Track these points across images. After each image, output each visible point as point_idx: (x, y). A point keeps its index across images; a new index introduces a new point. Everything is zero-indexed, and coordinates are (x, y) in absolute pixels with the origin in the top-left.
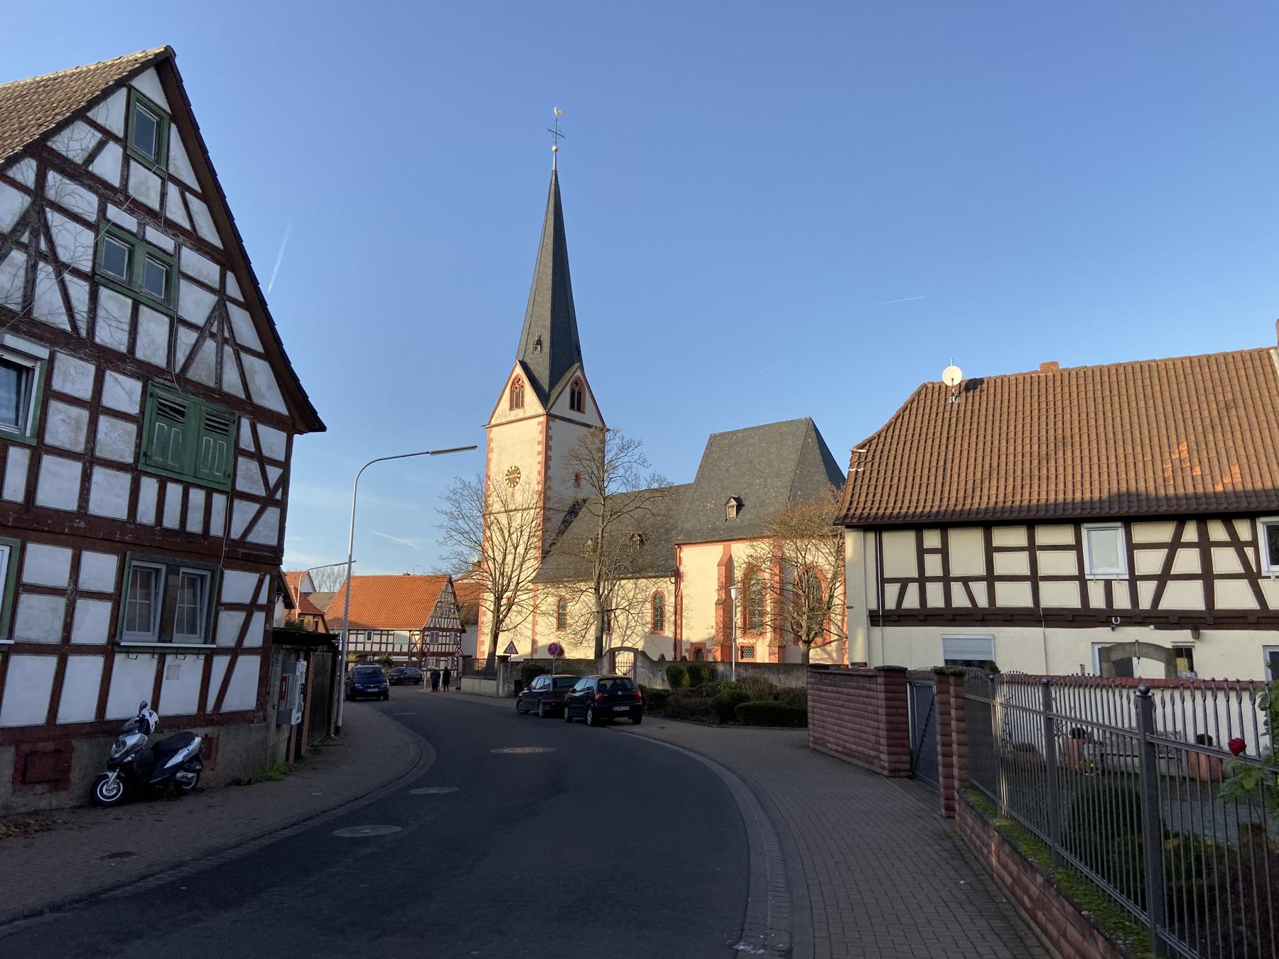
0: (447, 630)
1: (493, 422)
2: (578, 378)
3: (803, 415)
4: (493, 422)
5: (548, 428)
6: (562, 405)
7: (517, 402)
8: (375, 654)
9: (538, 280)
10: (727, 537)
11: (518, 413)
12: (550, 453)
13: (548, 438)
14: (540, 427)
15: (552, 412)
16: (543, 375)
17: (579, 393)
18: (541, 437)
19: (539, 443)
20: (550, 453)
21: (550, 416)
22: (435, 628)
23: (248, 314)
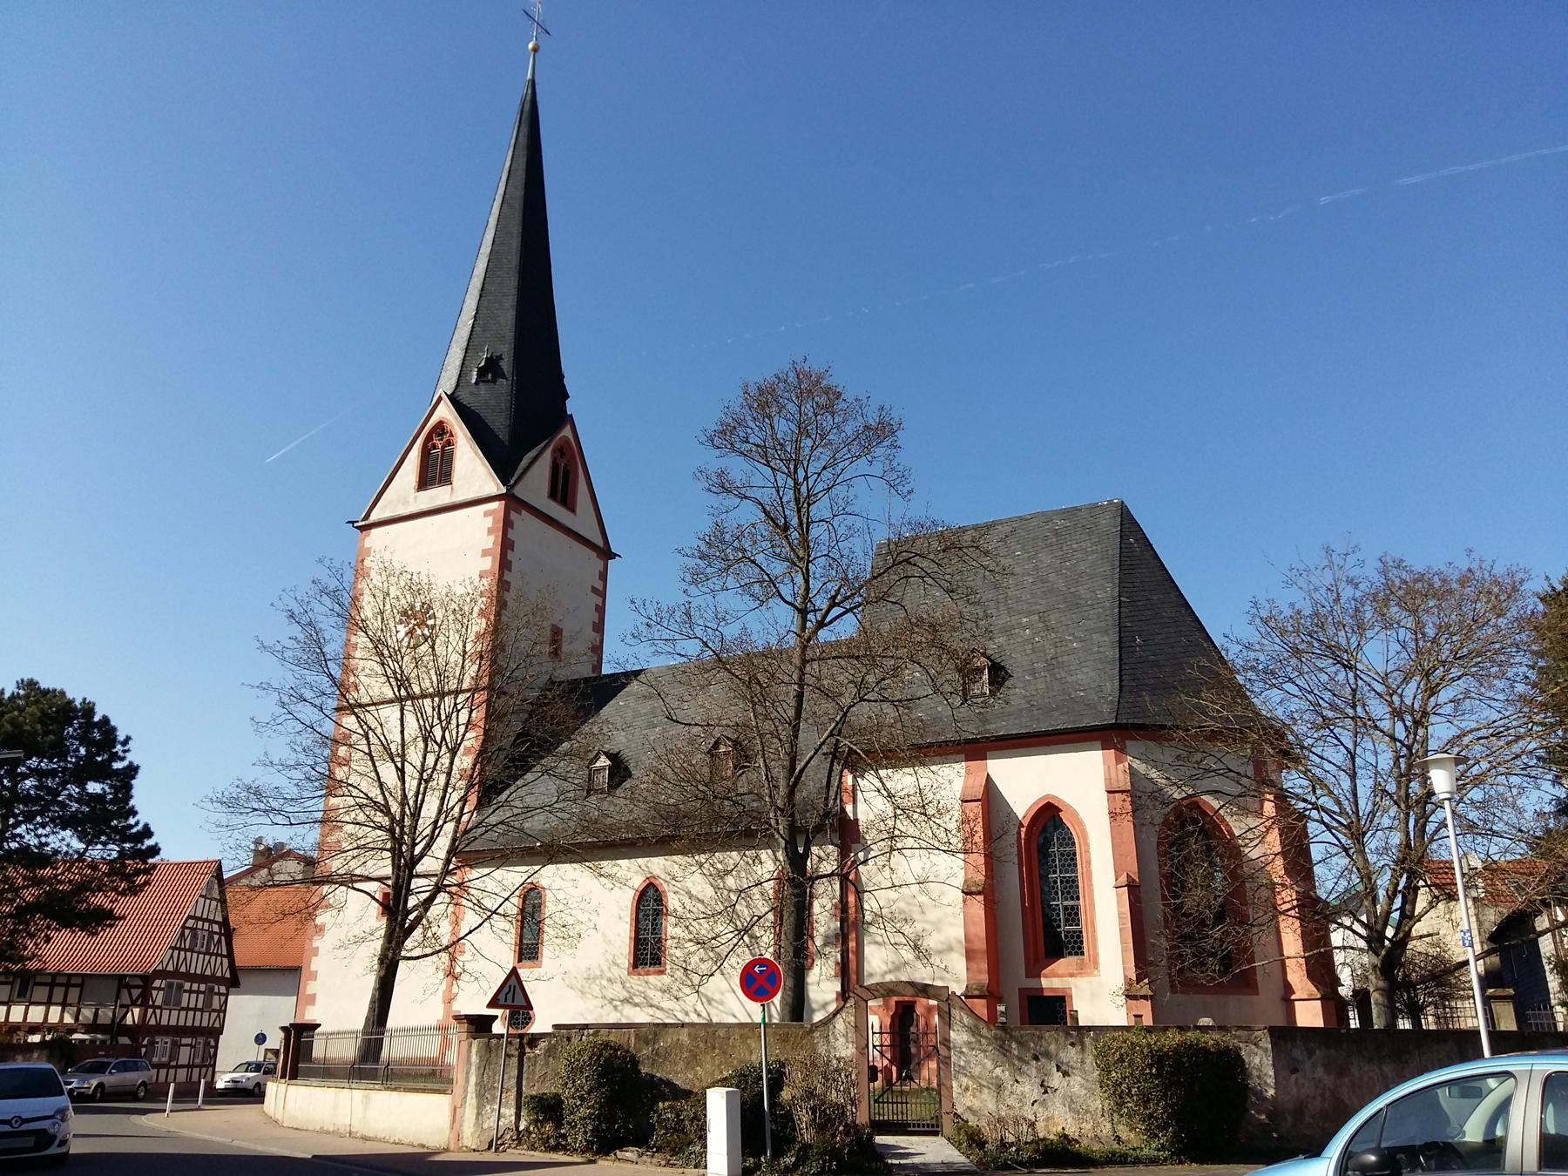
0: (200, 978)
1: (374, 517)
2: (566, 440)
3: (1106, 494)
4: (374, 517)
5: (507, 524)
6: (536, 482)
7: (435, 470)
8: (34, 1029)
9: (183, 1139)
10: (975, 749)
11: (438, 495)
12: (507, 576)
13: (506, 545)
14: (489, 522)
15: (518, 491)
16: (499, 423)
17: (566, 473)
18: (491, 542)
19: (485, 553)
20: (507, 576)
21: (512, 502)
22: (176, 973)
23: (630, 1153)
